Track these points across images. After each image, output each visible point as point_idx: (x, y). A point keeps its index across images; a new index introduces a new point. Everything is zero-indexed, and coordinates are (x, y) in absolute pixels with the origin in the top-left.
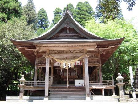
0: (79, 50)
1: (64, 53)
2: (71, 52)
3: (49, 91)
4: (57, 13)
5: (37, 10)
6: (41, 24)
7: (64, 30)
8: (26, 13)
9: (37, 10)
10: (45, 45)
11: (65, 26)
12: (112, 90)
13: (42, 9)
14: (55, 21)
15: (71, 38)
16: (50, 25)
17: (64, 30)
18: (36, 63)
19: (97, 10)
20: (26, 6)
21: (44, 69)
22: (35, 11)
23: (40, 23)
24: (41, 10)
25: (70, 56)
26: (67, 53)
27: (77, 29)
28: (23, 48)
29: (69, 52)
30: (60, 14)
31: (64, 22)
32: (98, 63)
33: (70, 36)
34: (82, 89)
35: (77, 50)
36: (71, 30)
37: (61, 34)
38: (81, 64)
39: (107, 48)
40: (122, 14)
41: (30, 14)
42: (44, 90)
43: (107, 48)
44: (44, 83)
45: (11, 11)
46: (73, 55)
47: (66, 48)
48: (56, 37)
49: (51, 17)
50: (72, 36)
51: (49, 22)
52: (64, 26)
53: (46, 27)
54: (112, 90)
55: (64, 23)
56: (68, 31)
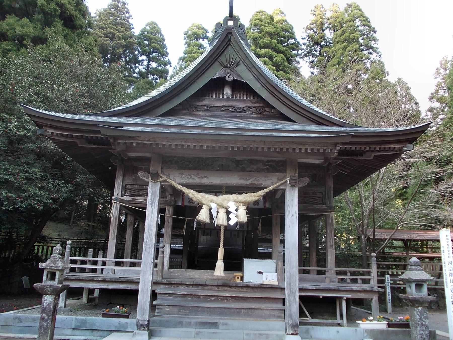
0: (268, 161)
3: (154, 295)
4: (194, 36)
6: (148, 65)
7: (217, 85)
10: (55, 240)
11: (221, 73)
14: (187, 59)
15: (239, 115)
16: (171, 71)
17: (217, 85)
18: (115, 194)
19: (308, 36)
20: (105, 10)
21: (139, 215)
22: (129, 28)
23: (145, 63)
27: (259, 85)
30: (201, 41)
31: (216, 60)
32: (324, 204)
33: (236, 110)
34: (270, 295)
35: (261, 161)
36: (239, 87)
37: (207, 102)
38: (268, 206)
39: (361, 158)
40: (378, 50)
42: (137, 291)
43: (361, 158)
48: (187, 108)
49: (175, 49)
50: (243, 110)
51: (170, 63)
52: (216, 72)
53: (162, 74)
55: (217, 63)
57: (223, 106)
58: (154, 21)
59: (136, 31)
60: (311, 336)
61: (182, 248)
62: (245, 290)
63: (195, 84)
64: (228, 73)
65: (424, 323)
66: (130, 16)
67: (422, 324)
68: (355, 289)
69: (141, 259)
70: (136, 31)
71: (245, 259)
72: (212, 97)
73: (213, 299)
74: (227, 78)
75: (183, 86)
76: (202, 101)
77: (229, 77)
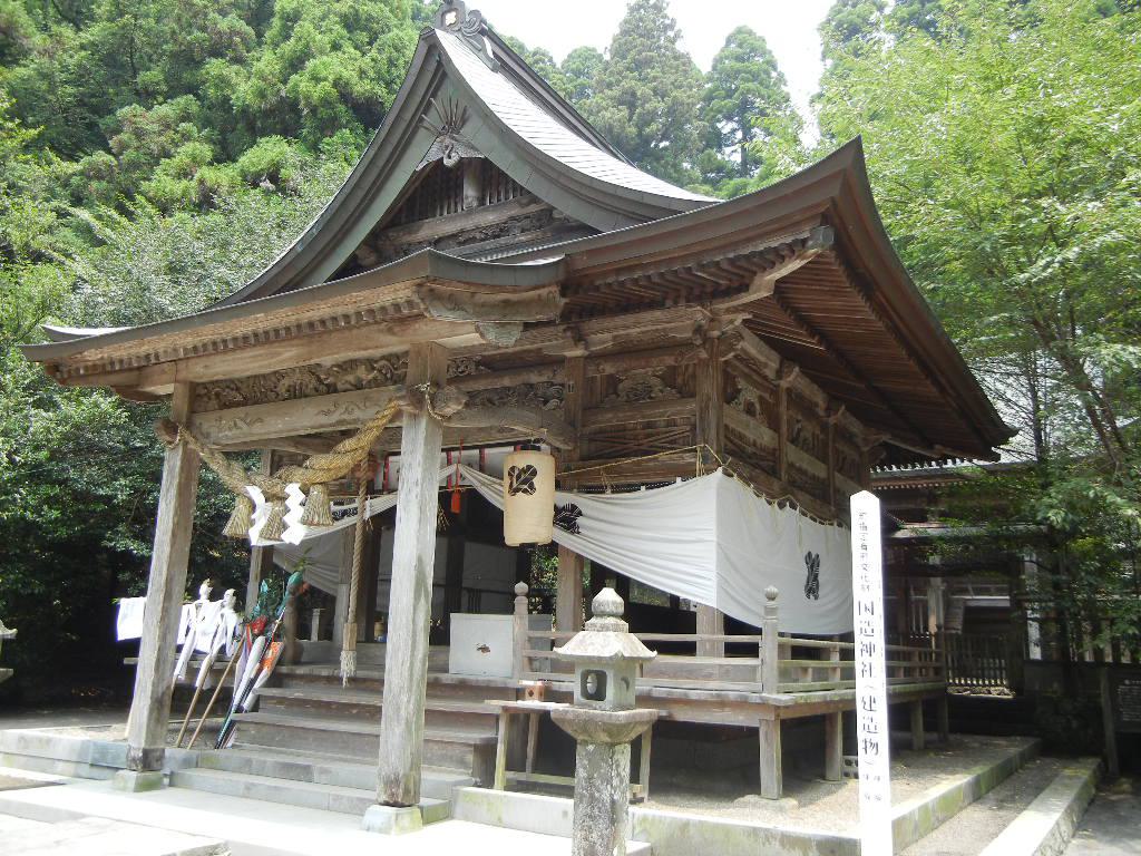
1: (278, 398)
2: (321, 385)
5: (702, 47)
8: (616, 92)
9: (702, 47)
12: (752, 734)
13: (740, 31)
24: (729, 41)
25: (306, 423)
26: (296, 394)
28: (886, 304)
29: (472, 369)
41: (642, 90)
44: (374, 713)
45: (323, 113)
46: (327, 413)
47: (286, 357)
54: (752, 734)
55: (422, 133)
56: (470, 192)
57: (462, 231)
58: (741, 24)
59: (703, 63)
60: (500, 819)
61: (1008, 604)
62: (439, 693)
63: (383, 193)
64: (447, 147)
65: (597, 795)
66: (677, 36)
67: (592, 796)
68: (693, 695)
69: (694, 631)
70: (703, 63)
71: (452, 615)
72: (441, 215)
73: (354, 711)
74: (447, 162)
75: (352, 206)
76: (417, 231)
77: (450, 157)
